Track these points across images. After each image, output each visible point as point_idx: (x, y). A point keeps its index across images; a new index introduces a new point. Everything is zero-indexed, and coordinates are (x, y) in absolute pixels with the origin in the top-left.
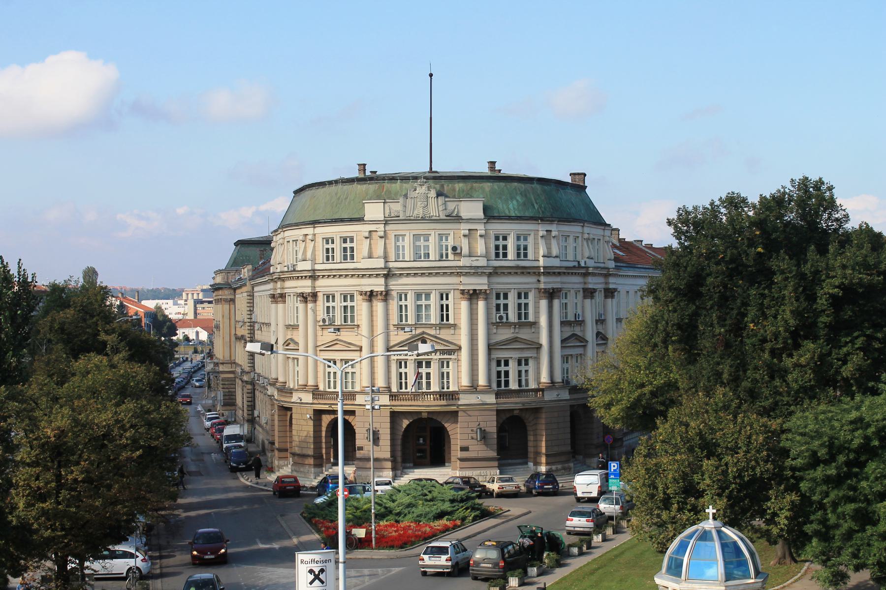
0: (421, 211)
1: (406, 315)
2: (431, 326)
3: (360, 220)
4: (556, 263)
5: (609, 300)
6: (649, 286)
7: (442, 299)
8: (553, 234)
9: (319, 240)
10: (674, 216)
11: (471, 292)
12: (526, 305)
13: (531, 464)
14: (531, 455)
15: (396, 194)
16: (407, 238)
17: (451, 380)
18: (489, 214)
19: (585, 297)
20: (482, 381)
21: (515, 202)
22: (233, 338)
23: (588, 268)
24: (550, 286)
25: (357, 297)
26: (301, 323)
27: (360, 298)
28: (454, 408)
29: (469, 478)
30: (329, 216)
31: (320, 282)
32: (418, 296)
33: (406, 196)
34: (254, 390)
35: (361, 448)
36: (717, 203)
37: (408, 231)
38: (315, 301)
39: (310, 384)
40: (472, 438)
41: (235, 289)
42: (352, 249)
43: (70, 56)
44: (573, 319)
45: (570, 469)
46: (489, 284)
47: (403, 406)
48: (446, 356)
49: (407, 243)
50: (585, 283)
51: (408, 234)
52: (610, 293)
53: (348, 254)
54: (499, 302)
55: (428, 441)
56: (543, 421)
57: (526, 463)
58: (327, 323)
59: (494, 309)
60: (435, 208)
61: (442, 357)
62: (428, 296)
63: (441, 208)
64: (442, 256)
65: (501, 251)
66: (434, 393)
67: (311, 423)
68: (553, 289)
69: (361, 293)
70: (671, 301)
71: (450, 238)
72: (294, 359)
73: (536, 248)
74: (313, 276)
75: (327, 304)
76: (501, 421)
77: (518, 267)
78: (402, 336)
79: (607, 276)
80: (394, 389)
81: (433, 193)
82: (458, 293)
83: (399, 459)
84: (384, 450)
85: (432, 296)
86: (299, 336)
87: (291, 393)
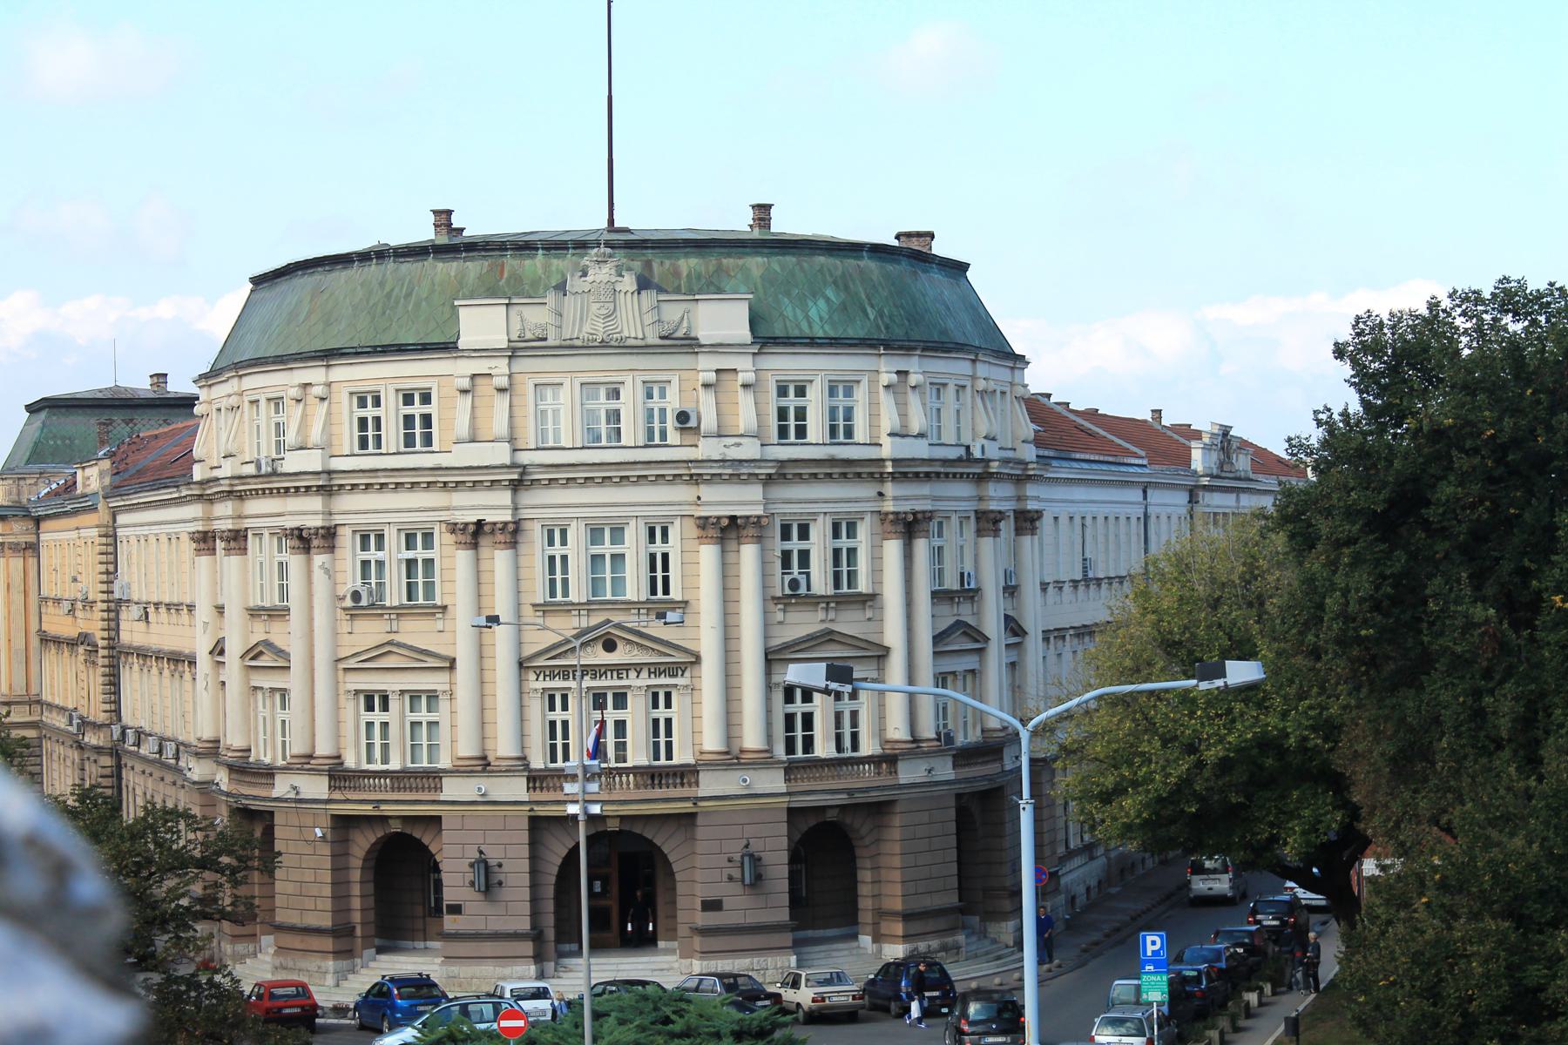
0: (600, 326)
1: (565, 582)
2: (629, 605)
3: (448, 347)
4: (920, 450)
5: (1026, 540)
6: (1281, 509)
8: (913, 379)
10: (1346, 334)
11: (725, 522)
12: (852, 552)
13: (866, 940)
14: (866, 917)
15: (535, 283)
17: (675, 739)
18: (765, 338)
19: (980, 533)
20: (752, 738)
21: (822, 303)
22: (35, 642)
23: (986, 462)
24: (472, 517)
25: (442, 538)
26: (295, 602)
27: (449, 539)
28: (686, 807)
29: (735, 976)
30: (364, 339)
31: (346, 502)
32: (595, 534)
33: (561, 288)
34: (119, 767)
35: (456, 909)
36: (1446, 303)
37: (570, 373)
38: (331, 549)
39: (318, 753)
41: (38, 521)
42: (427, 420)
44: (956, 587)
45: (958, 948)
46: (767, 502)
48: (558, 683)
50: (981, 499)
51: (567, 383)
52: (1027, 521)
53: (418, 431)
54: (787, 546)
55: (615, 889)
56: (896, 834)
57: (855, 937)
58: (364, 603)
59: (778, 563)
60: (635, 316)
61: (654, 681)
62: (618, 533)
63: (648, 319)
64: (651, 436)
65: (792, 423)
66: (636, 770)
67: (326, 850)
68: (915, 514)
69: (453, 528)
70: (1350, 541)
71: (673, 393)
72: (273, 690)
73: (874, 416)
74: (327, 486)
76: (797, 837)
77: (832, 461)
78: (566, 626)
79: (1021, 480)
81: (628, 282)
82: (690, 525)
83: (550, 934)
85: (629, 534)
86: (288, 636)
87: (272, 776)
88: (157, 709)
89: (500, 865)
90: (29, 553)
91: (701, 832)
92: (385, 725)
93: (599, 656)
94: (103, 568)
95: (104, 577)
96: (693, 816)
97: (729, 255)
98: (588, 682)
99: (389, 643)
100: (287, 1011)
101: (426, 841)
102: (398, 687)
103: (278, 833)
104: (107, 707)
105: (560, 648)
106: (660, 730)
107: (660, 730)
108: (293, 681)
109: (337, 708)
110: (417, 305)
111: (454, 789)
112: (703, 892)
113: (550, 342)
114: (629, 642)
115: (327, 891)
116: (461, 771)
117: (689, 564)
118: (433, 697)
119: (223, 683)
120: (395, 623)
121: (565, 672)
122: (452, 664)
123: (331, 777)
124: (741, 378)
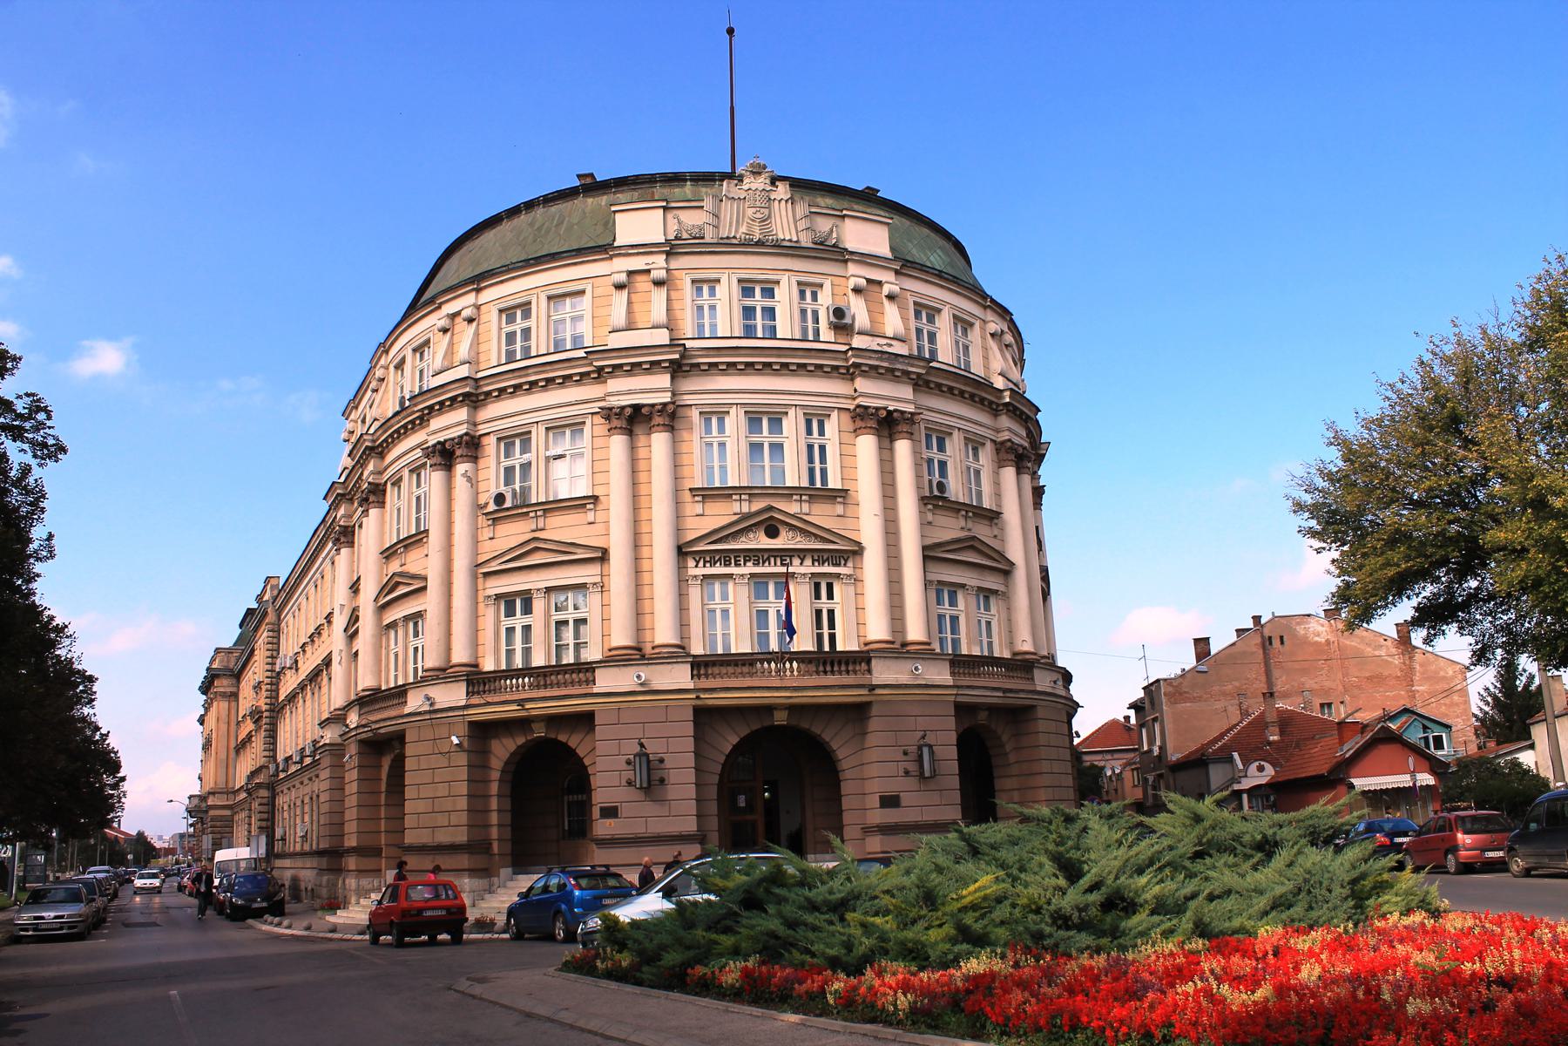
2: (789, 493)
3: (606, 249)
7: (809, 432)
9: (491, 316)
11: (883, 414)
16: (721, 290)
32: (754, 419)
34: (274, 798)
35: (610, 812)
37: (729, 270)
38: (474, 459)
39: (456, 659)
43: (54, 590)
47: (731, 691)
48: (827, 569)
49: (727, 296)
58: (508, 504)
63: (802, 225)
66: (802, 657)
67: (462, 759)
78: (720, 515)
84: (681, 808)
86: (425, 562)
88: (301, 733)
89: (662, 761)
91: (874, 724)
92: (527, 629)
93: (762, 541)
96: (869, 704)
98: (750, 569)
100: (429, 913)
101: (573, 743)
102: (543, 585)
103: (409, 764)
105: (716, 535)
108: (430, 603)
109: (475, 616)
110: (570, 228)
111: (607, 680)
112: (877, 787)
113: (708, 239)
114: (792, 527)
115: (463, 803)
116: (616, 659)
117: (846, 456)
119: (356, 654)
120: (541, 520)
121: (727, 557)
122: (603, 556)
123: (469, 683)
124: (886, 289)
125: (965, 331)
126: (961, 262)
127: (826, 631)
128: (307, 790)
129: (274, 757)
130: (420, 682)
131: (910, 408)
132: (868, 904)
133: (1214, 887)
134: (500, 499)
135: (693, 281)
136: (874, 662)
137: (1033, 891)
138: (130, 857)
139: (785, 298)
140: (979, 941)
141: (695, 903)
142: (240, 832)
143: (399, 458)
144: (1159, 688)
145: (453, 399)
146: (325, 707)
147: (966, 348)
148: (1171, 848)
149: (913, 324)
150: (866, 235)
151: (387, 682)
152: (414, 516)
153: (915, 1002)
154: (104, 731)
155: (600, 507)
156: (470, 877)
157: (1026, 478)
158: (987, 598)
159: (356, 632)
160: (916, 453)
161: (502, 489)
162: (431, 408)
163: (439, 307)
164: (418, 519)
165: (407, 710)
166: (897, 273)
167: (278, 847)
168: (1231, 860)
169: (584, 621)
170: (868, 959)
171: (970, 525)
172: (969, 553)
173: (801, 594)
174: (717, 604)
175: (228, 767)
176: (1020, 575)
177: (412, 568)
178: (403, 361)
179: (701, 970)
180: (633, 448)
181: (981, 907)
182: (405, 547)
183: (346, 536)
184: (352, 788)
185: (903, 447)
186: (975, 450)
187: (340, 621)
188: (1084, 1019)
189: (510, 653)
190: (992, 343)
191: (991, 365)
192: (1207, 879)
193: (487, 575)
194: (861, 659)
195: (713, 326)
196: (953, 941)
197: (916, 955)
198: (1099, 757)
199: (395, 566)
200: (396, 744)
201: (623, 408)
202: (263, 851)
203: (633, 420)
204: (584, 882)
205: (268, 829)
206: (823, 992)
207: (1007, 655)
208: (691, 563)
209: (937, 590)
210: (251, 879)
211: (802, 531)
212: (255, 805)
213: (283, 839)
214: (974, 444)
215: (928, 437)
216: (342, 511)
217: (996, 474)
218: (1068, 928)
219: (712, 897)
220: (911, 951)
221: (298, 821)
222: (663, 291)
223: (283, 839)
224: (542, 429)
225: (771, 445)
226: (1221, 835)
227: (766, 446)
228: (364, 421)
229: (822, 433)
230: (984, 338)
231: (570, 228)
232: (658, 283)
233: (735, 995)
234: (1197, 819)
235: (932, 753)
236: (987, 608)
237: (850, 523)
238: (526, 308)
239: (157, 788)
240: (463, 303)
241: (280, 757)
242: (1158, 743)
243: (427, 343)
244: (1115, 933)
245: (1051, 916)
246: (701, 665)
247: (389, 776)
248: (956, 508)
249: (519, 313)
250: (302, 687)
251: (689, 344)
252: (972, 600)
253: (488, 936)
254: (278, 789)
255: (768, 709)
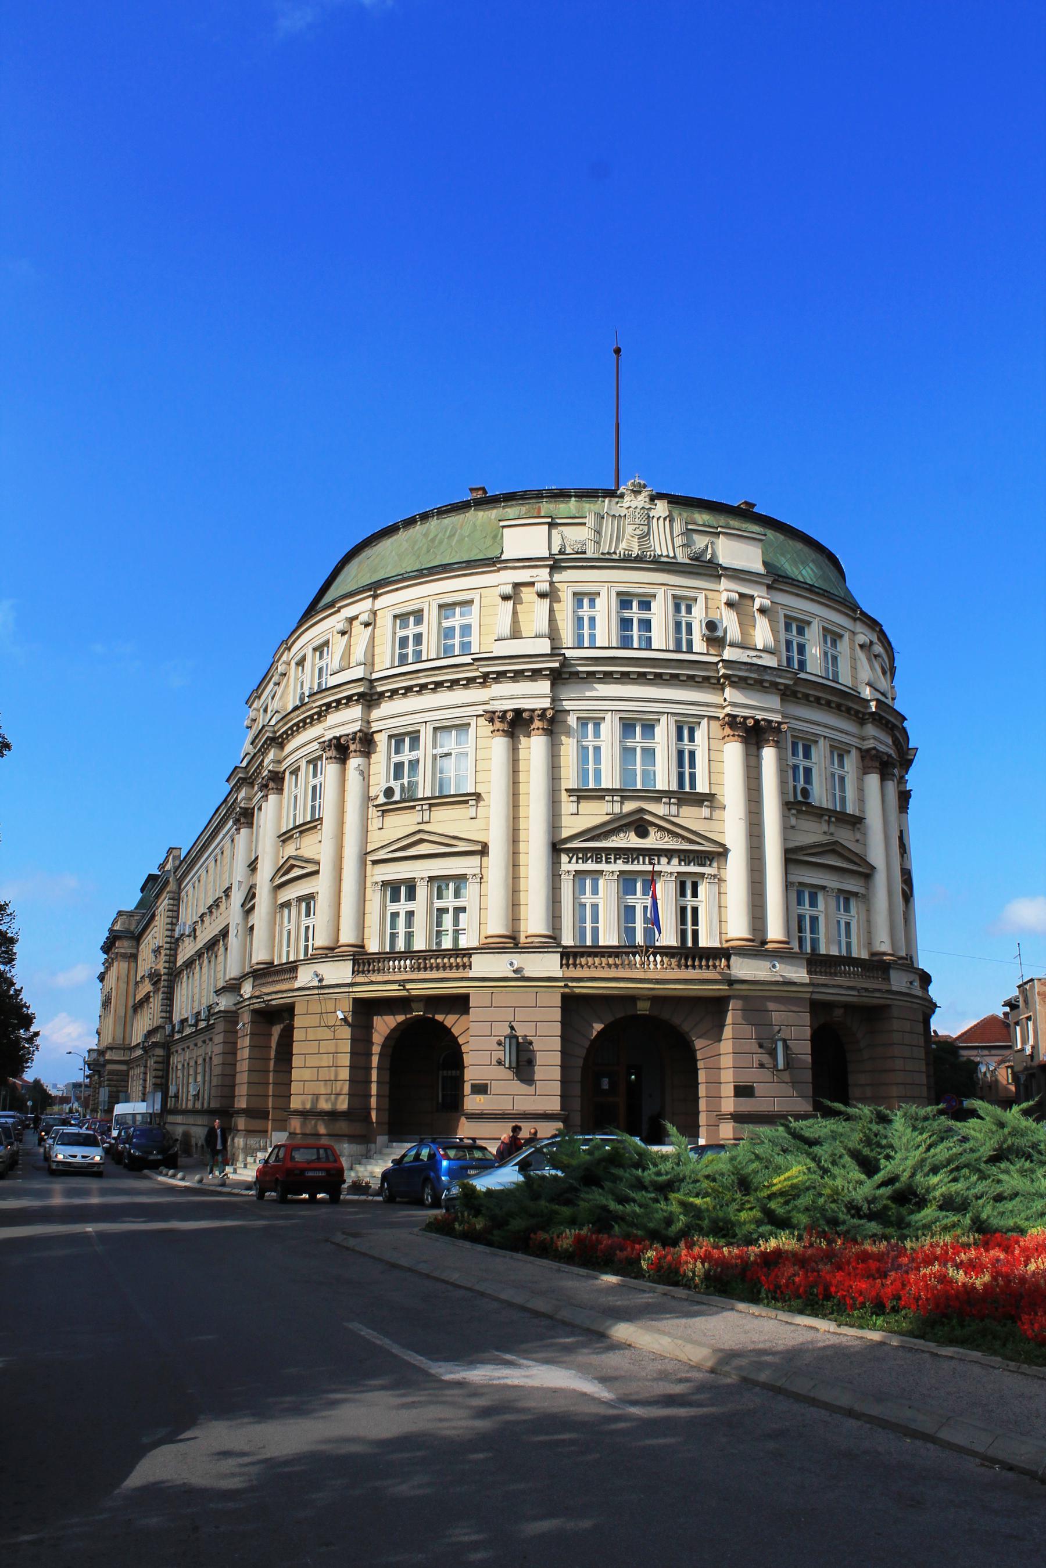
2: (658, 796)
3: (493, 563)
7: (680, 738)
9: (385, 621)
11: (750, 723)
20: (775, 931)
26: (328, 814)
31: (387, 708)
32: (627, 726)
35: (480, 1089)
40: (762, 1066)
47: (598, 978)
48: (693, 868)
49: (604, 614)
58: (397, 797)
62: (649, 728)
63: (678, 541)
66: (667, 952)
67: (346, 1032)
75: (396, 759)
78: (595, 813)
80: (568, 939)
84: (546, 1092)
85: (660, 731)
86: (316, 847)
88: (196, 997)
90: (132, 959)
92: (410, 914)
93: (631, 840)
94: (169, 920)
95: (169, 927)
97: (734, 519)
98: (620, 866)
99: (419, 831)
100: (310, 1174)
103: (297, 1035)
104: (164, 1014)
106: (687, 916)
107: (687, 916)
108: (321, 886)
110: (461, 539)
113: (589, 555)
114: (661, 828)
118: (460, 879)
119: (252, 928)
121: (597, 854)
122: (483, 851)
123: (355, 962)
124: (758, 603)
125: (834, 643)
126: (832, 574)
127: (689, 927)
128: (201, 1051)
129: (170, 1018)
130: (310, 960)
131: (777, 718)
132: (691, 1186)
133: (1006, 1188)
134: (389, 792)
135: (575, 594)
136: (733, 958)
137: (839, 1182)
138: (29, 1103)
139: (660, 613)
140: (782, 1223)
141: (544, 1177)
142: (135, 1087)
143: (297, 749)
144: (1033, 987)
145: (349, 698)
146: (220, 975)
147: (835, 659)
148: (972, 1150)
149: (783, 636)
150: (738, 552)
151: (280, 957)
152: (310, 804)
153: (709, 1270)
154: (17, 987)
155: (481, 804)
156: (350, 1142)
157: (891, 787)
158: (847, 901)
159: (253, 907)
160: (781, 760)
161: (392, 783)
162: (328, 705)
163: (338, 611)
164: (313, 807)
165: (297, 985)
166: (769, 587)
167: (171, 1103)
168: (1028, 1165)
169: (463, 909)
170: (685, 1233)
171: (832, 829)
172: (827, 854)
173: (666, 891)
174: (588, 899)
175: (126, 1024)
176: (880, 879)
177: (307, 852)
178: (304, 659)
179: (543, 1236)
180: (514, 750)
181: (791, 1194)
182: (301, 832)
183: (246, 817)
184: (244, 1054)
185: (769, 755)
186: (841, 757)
187: (237, 897)
188: (833, 1289)
189: (393, 936)
190: (861, 656)
191: (859, 676)
192: (999, 1181)
193: (375, 862)
194: (723, 953)
195: (592, 637)
196: (759, 1223)
197: (723, 1230)
198: (974, 1052)
199: (290, 850)
200: (286, 1015)
201: (505, 712)
202: (158, 1107)
203: (515, 724)
204: (452, 1153)
205: (162, 1085)
206: (638, 1259)
207: (865, 955)
208: (564, 858)
209: (796, 892)
210: (144, 1133)
211: (669, 832)
212: (151, 1063)
213: (176, 1096)
214: (839, 751)
215: (794, 745)
216: (242, 794)
217: (860, 781)
218: (860, 1217)
219: (559, 1173)
220: (722, 1229)
221: (191, 1080)
222: (546, 602)
223: (176, 1096)
224: (430, 728)
225: (643, 750)
226: (1022, 1142)
227: (638, 750)
228: (266, 711)
229: (692, 739)
230: (852, 649)
231: (461, 539)
232: (542, 595)
233: (568, 1258)
234: (1002, 1125)
235: (786, 1047)
236: (847, 909)
237: (714, 825)
238: (418, 615)
239: (63, 1041)
240: (362, 607)
241: (176, 1019)
242: (1031, 1042)
243: (326, 643)
244: (901, 1224)
245: (846, 1206)
246: (569, 956)
247: (278, 1044)
248: (820, 813)
249: (412, 619)
250: (199, 954)
251: (569, 653)
252: (833, 903)
253: (363, 1197)
254: (173, 1050)
255: (629, 999)
